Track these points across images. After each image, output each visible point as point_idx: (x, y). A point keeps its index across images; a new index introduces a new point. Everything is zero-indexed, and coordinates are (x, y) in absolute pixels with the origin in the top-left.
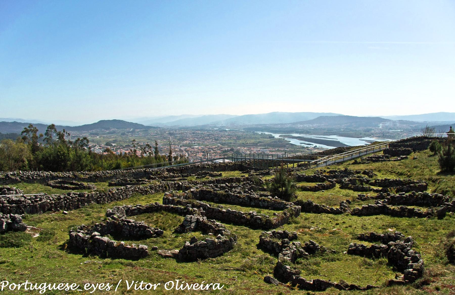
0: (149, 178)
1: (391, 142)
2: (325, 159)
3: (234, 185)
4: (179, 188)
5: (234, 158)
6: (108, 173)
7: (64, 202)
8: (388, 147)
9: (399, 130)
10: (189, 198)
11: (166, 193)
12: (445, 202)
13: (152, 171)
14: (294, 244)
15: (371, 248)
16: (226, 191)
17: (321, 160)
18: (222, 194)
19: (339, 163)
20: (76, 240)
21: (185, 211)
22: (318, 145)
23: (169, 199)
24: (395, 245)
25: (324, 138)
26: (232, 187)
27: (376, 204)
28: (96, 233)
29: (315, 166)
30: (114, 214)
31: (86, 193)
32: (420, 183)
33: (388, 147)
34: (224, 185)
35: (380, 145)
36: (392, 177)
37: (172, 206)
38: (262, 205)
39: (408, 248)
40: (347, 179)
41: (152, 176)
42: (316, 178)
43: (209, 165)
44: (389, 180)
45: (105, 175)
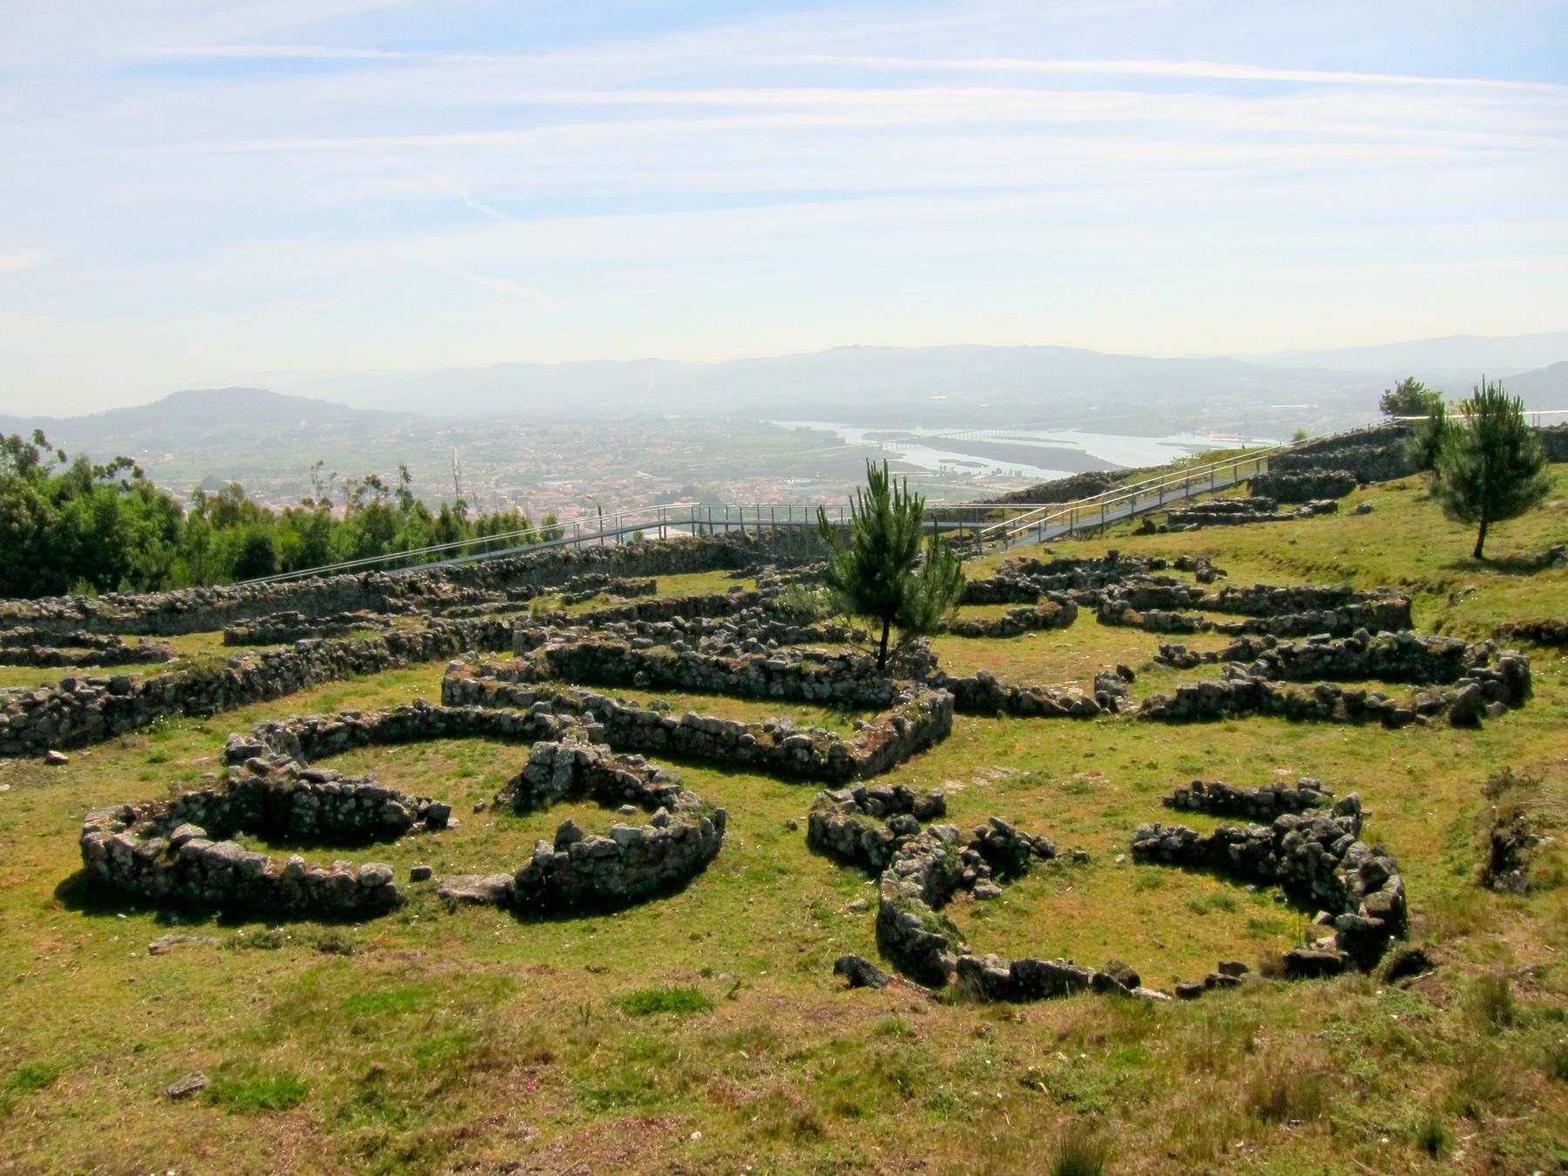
0: (383, 608)
1: (1276, 450)
2: (1031, 519)
3: (705, 621)
4: (496, 639)
5: (701, 523)
6: (219, 595)
7: (50, 717)
8: (1264, 471)
9: (1304, 406)
10: (540, 678)
11: (453, 662)
12: (1476, 665)
13: (393, 580)
14: (935, 835)
15: (1212, 840)
16: (679, 649)
17: (1021, 521)
18: (664, 659)
19: (1087, 533)
20: (110, 860)
21: (527, 727)
22: (1007, 467)
23: (464, 687)
24: (1300, 828)
25: (1020, 439)
26: (696, 633)
27: (1228, 679)
28: (188, 829)
29: (999, 543)
30: (256, 752)
31: (139, 675)
32: (1385, 598)
33: (1264, 471)
34: (669, 624)
35: (1235, 462)
36: (1284, 582)
37: (479, 709)
38: (810, 696)
39: (1348, 837)
40: (1116, 589)
41: (392, 600)
42: (1005, 589)
43: (607, 552)
44: (1272, 588)
45: (211, 604)
